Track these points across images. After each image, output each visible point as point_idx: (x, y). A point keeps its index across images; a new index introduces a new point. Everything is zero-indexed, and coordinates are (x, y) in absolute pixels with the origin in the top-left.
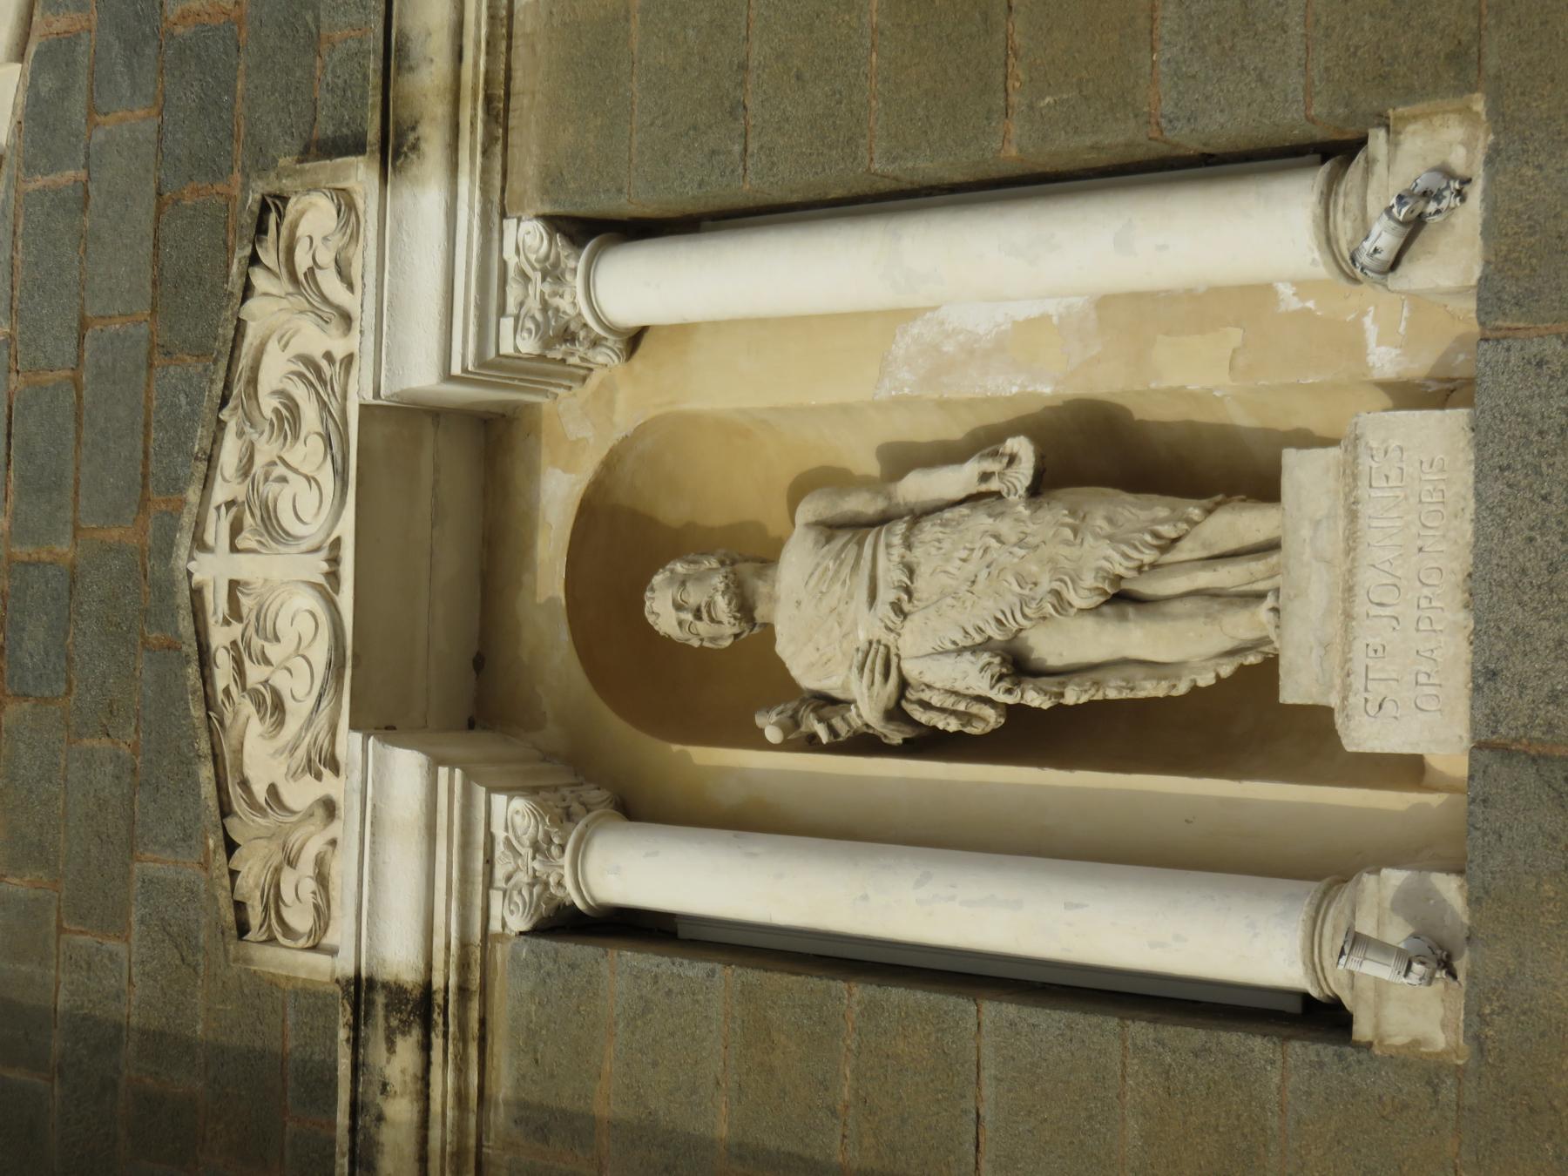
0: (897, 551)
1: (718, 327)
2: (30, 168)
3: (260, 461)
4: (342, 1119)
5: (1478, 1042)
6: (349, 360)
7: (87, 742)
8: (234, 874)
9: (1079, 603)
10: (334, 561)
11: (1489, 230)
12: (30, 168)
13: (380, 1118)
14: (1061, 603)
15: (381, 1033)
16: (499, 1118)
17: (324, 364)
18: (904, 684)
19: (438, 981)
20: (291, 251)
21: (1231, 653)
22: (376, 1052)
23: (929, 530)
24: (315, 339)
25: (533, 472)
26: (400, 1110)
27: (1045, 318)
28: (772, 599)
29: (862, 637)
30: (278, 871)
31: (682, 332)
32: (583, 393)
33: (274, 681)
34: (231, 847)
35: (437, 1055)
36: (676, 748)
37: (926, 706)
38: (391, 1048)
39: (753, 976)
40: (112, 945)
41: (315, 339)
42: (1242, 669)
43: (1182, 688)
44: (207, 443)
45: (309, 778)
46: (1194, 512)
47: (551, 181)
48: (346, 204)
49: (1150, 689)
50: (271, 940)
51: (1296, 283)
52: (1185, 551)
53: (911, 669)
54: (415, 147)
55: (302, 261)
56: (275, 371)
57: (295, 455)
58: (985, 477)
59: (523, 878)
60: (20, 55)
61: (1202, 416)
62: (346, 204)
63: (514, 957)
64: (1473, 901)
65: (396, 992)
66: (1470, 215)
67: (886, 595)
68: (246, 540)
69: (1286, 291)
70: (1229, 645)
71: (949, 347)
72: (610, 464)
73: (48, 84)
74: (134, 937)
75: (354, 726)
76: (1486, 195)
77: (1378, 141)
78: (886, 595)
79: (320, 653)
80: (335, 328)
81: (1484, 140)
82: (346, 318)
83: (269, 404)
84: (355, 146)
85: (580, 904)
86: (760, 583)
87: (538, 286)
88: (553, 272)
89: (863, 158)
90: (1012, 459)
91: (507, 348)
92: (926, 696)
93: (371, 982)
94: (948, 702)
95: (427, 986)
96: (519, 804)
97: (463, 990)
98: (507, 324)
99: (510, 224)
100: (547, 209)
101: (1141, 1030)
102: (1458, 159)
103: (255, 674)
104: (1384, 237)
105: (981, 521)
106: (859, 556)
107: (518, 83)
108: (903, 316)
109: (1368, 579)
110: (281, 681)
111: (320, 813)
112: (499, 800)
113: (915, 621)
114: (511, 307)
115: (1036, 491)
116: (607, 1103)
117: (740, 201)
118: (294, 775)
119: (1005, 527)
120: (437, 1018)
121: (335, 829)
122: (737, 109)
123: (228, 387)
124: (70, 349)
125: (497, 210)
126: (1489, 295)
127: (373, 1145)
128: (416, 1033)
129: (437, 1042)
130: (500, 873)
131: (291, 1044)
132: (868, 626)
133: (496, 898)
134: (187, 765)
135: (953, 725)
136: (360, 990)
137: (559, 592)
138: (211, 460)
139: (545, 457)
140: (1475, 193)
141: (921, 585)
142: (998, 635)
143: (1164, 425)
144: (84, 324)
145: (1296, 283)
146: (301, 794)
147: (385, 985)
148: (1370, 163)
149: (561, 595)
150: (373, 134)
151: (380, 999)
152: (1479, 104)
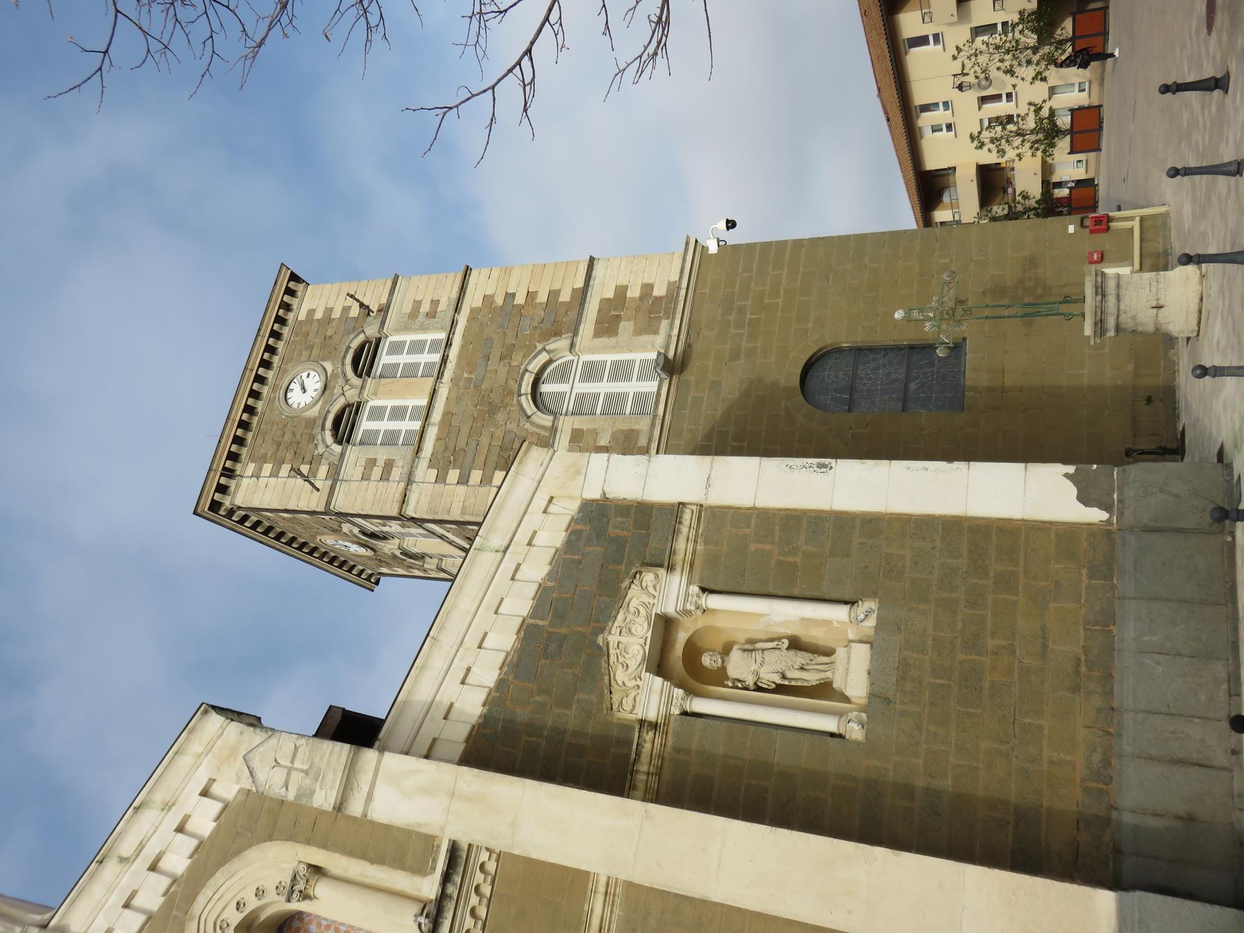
0: (761, 655)
1: (721, 610)
2: (566, 553)
3: (628, 620)
4: (634, 747)
5: (867, 739)
6: (654, 604)
7: (565, 670)
8: (611, 698)
9: (796, 667)
10: (646, 640)
11: (877, 619)
12: (566, 553)
13: (643, 747)
14: (793, 667)
15: (645, 730)
16: (668, 749)
17: (648, 604)
18: (759, 678)
19: (659, 722)
20: (642, 582)
21: (818, 680)
22: (644, 734)
23: (766, 652)
24: (645, 599)
25: (677, 632)
26: (648, 746)
27: (790, 621)
28: (728, 662)
29: (753, 669)
30: (622, 698)
31: (714, 611)
32: (690, 619)
33: (627, 661)
34: (611, 693)
35: (657, 736)
36: (705, 686)
37: (762, 682)
38: (647, 733)
39: (730, 724)
40: (566, 712)
41: (645, 599)
42: (820, 683)
43: (811, 684)
44: (616, 614)
45: (634, 680)
46: (816, 656)
47: (701, 580)
48: (657, 576)
49: (806, 684)
50: (619, 711)
51: (837, 622)
52: (813, 662)
53: (761, 675)
54: (674, 569)
55: (644, 584)
56: (634, 603)
57: (637, 620)
58: (778, 645)
59: (679, 704)
60: (566, 531)
61: (814, 641)
62: (657, 576)
63: (676, 719)
64: (868, 717)
65: (650, 723)
66: (875, 616)
67: (758, 662)
68: (623, 634)
69: (835, 623)
70: (819, 678)
71: (771, 622)
72: (694, 633)
73: (573, 538)
74: (573, 712)
75: (646, 671)
76: (877, 614)
77: (860, 602)
78: (758, 662)
79: (639, 658)
80: (652, 598)
81: (877, 606)
82: (654, 597)
83: (632, 609)
84: (661, 566)
85: (689, 711)
86: (444, 703)
87: (695, 598)
88: (698, 596)
89: (351, 531)
90: (783, 643)
91: (688, 608)
92: (762, 681)
93: (645, 720)
94: (767, 682)
95: (657, 722)
96: (680, 690)
97: (664, 724)
98: (689, 604)
99: (691, 586)
100: (700, 585)
101: (808, 736)
102: (873, 608)
103: (621, 659)
104: (862, 616)
105: (777, 652)
106: (751, 656)
107: (696, 562)
108: (762, 615)
109: (851, 668)
110: (628, 662)
111: (637, 687)
112: (676, 689)
113: (764, 667)
114: (689, 601)
115: (787, 649)
116: (694, 746)
117: (741, 592)
118: (630, 680)
119: (782, 653)
120: (658, 728)
121: (640, 691)
122: (743, 576)
123: (622, 605)
124: (573, 590)
125: (689, 583)
126: (876, 628)
127: (640, 752)
128: (654, 731)
129: (657, 733)
130: (674, 703)
131: (615, 734)
132: (754, 667)
133: (673, 708)
134: (603, 675)
135: (766, 687)
136: (642, 722)
137: (680, 654)
138: (616, 618)
139: (680, 629)
140: (876, 613)
141: (766, 661)
142: (781, 671)
143: (805, 642)
144: (576, 587)
145: (837, 622)
146: (631, 684)
147: (648, 721)
148: (858, 606)
149: (681, 655)
150: (666, 564)
151: (646, 724)
152: (877, 600)
